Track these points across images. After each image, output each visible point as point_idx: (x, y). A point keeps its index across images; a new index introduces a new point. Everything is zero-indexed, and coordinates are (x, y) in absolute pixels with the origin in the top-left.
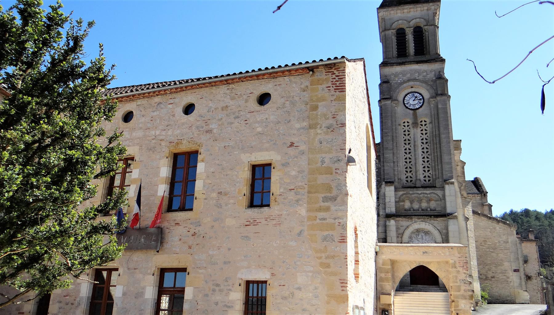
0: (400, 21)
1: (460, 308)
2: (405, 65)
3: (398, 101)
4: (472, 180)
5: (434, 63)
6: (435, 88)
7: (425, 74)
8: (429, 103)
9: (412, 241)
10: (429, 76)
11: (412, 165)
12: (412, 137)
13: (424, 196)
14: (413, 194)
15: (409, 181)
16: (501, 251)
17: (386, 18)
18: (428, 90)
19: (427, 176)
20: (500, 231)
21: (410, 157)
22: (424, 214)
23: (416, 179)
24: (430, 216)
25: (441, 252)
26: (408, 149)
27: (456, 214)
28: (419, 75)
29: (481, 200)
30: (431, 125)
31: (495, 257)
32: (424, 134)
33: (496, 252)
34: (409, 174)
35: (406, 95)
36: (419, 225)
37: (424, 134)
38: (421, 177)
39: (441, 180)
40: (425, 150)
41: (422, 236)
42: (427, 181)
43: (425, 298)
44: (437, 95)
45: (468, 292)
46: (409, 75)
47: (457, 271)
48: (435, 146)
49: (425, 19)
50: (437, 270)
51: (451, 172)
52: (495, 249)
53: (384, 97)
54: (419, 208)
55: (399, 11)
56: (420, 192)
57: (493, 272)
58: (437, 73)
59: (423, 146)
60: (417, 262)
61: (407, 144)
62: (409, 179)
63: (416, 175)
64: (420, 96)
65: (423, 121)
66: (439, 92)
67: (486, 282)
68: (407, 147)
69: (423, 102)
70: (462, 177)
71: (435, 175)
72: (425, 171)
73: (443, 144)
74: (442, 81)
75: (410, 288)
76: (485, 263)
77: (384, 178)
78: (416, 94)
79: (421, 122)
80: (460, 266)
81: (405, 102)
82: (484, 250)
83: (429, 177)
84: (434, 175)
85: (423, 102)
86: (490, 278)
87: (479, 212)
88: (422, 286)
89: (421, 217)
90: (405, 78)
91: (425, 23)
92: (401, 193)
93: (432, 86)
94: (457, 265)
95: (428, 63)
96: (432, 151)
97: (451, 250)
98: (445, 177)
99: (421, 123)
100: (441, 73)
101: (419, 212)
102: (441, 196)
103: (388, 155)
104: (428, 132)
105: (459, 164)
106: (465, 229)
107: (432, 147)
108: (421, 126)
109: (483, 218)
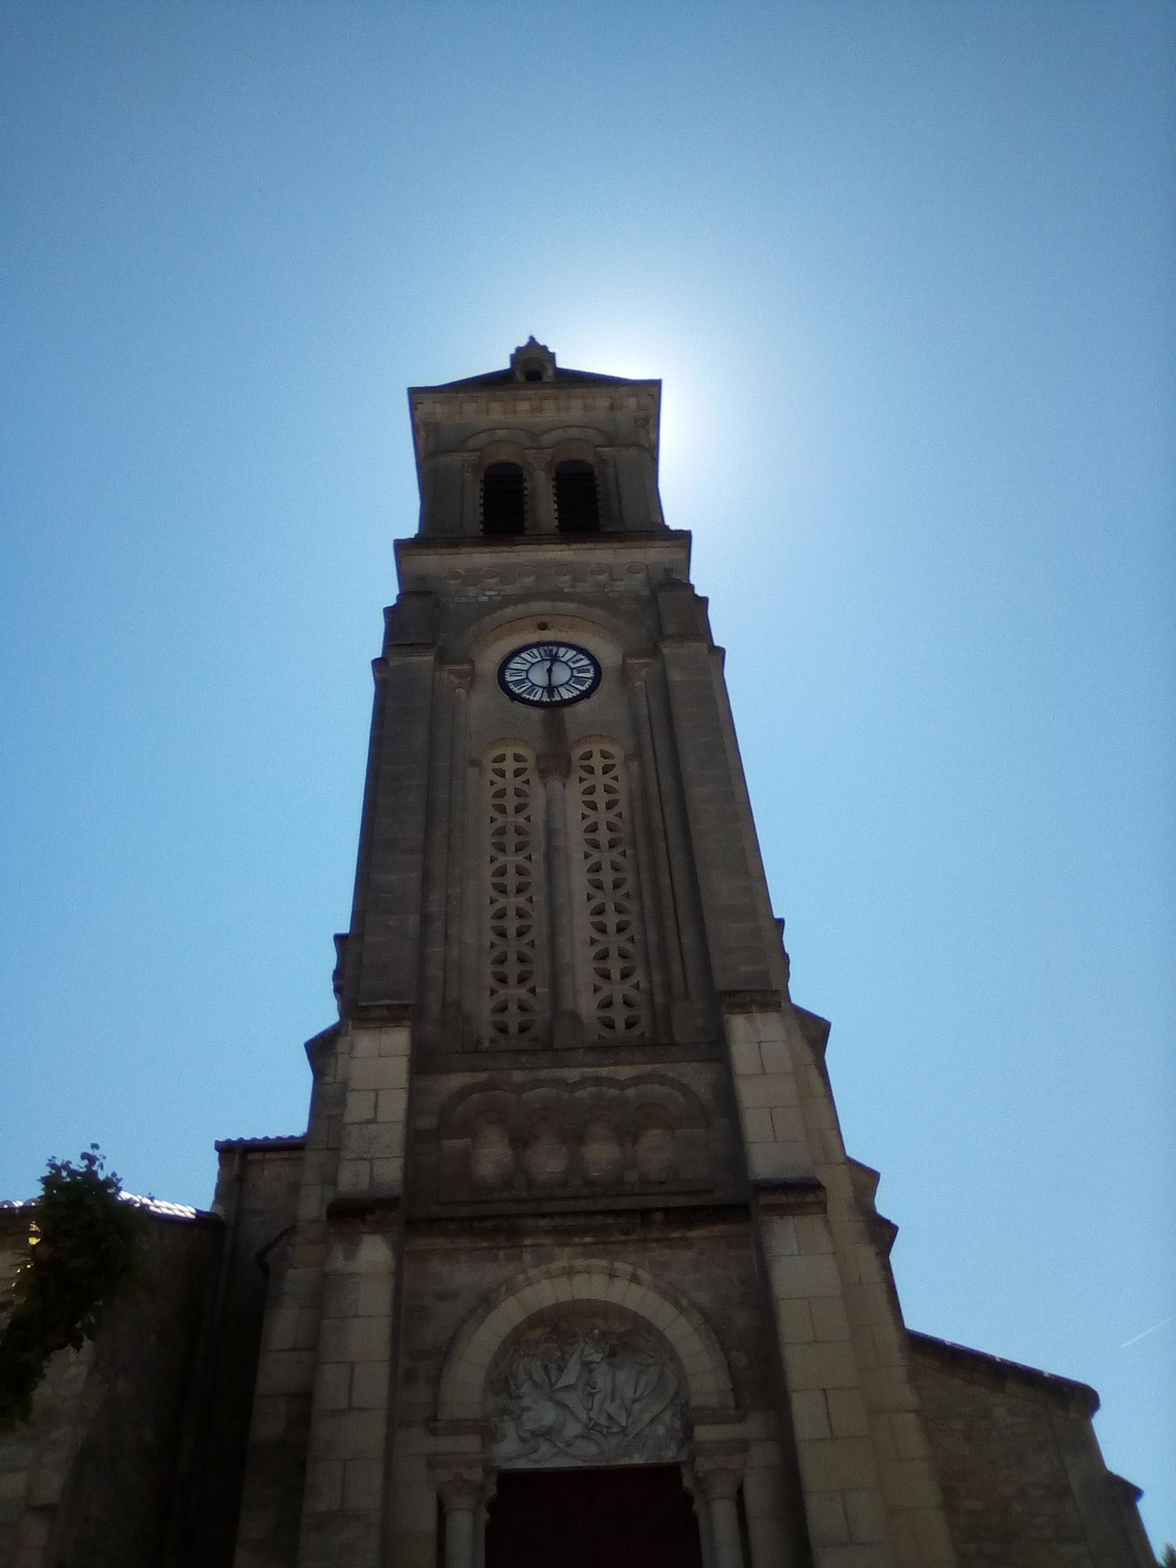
7: (603, 578)
10: (620, 586)
12: (538, 818)
14: (537, 1084)
30: (634, 765)
34: (515, 993)
38: (587, 1006)
41: (587, 1366)
42: (620, 1023)
46: (529, 581)
48: (662, 844)
49: (600, 431)
62: (513, 1019)
68: (511, 860)
71: (668, 987)
81: (509, 679)
90: (509, 590)
92: (455, 1082)
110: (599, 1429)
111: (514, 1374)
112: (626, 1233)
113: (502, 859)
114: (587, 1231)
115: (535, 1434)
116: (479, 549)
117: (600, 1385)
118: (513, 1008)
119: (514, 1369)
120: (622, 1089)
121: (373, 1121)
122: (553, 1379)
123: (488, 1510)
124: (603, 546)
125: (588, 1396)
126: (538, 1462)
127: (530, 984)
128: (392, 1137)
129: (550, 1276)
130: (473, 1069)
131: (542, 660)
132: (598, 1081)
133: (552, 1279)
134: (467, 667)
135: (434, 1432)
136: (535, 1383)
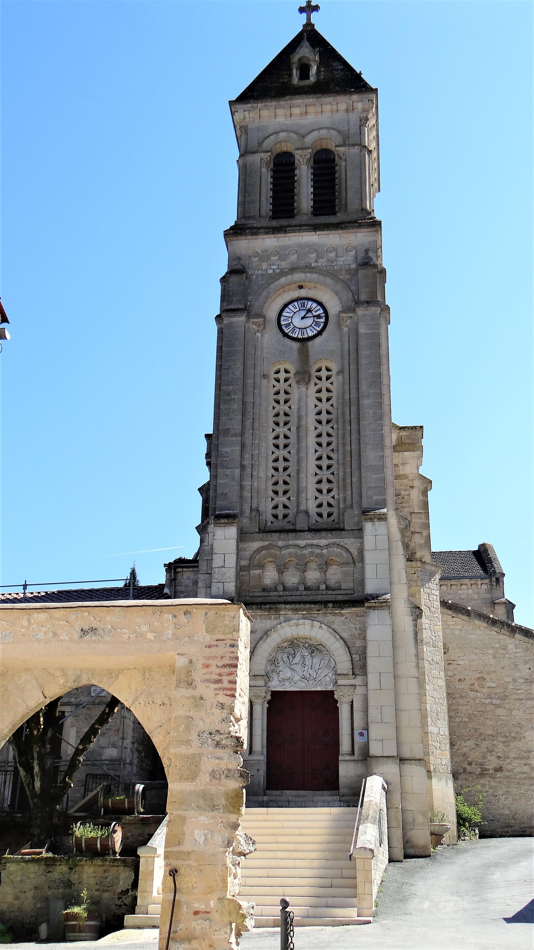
0: (283, 135)
1: (187, 846)
2: (286, 232)
3: (264, 317)
4: (474, 550)
5: (356, 230)
6: (353, 288)
8: (339, 325)
9: (277, 670)
11: (289, 475)
13: (312, 554)
14: (287, 547)
15: (280, 517)
16: (518, 704)
17: (250, 126)
18: (336, 293)
19: (325, 504)
20: (517, 655)
21: (288, 456)
22: (311, 598)
23: (298, 512)
24: (325, 603)
25: (145, 628)
26: (282, 436)
27: (388, 596)
28: (318, 257)
29: (491, 593)
30: (340, 377)
31: (505, 718)
32: (324, 400)
33: (507, 706)
34: (282, 499)
35: (286, 306)
36: (295, 627)
37: (324, 400)
38: (312, 506)
39: (356, 512)
40: (324, 440)
41: (303, 657)
42: (325, 515)
43: (279, 824)
44: (358, 303)
45: (224, 781)
46: (294, 258)
47: (194, 697)
48: (348, 428)
49: (339, 131)
50: (136, 698)
51: (383, 490)
52: (504, 698)
53: (229, 307)
54: (299, 583)
55: (280, 112)
56: (302, 543)
57: (499, 757)
58: (362, 255)
59: (320, 428)
60: (70, 673)
61: (282, 424)
62: (281, 512)
63: (297, 499)
64: (319, 307)
65: (324, 369)
66: (363, 297)
67: (482, 781)
68: (281, 430)
69: (326, 323)
70: (423, 516)
71: (345, 500)
72: (320, 491)
73: (365, 422)
74: (370, 271)
75: (260, 798)
76: (481, 734)
77: (215, 508)
78: (310, 304)
79: (319, 370)
80: (208, 677)
81: (283, 323)
82: (478, 701)
83: (329, 505)
84: (341, 501)
85: (326, 323)
86: (491, 772)
87: (469, 608)
88: (295, 792)
89: (302, 606)
90: (284, 264)
91: (339, 140)
93: (346, 284)
94: (198, 675)
95: (342, 228)
96: (340, 440)
97: (183, 619)
98: (365, 505)
99: (318, 374)
100: (371, 254)
101: (298, 593)
102: (355, 552)
103: (228, 450)
104: (334, 395)
105: (417, 483)
106: (411, 635)
107: (340, 432)
108: (317, 381)
109: (477, 622)
112: (319, 610)
113: (278, 430)
116: (268, 236)
117: (307, 663)
118: (281, 507)
122: (291, 661)
123: (268, 703)
124: (333, 232)
127: (288, 495)
128: (231, 574)
130: (262, 540)
131: (300, 310)
132: (312, 545)
134: (261, 320)
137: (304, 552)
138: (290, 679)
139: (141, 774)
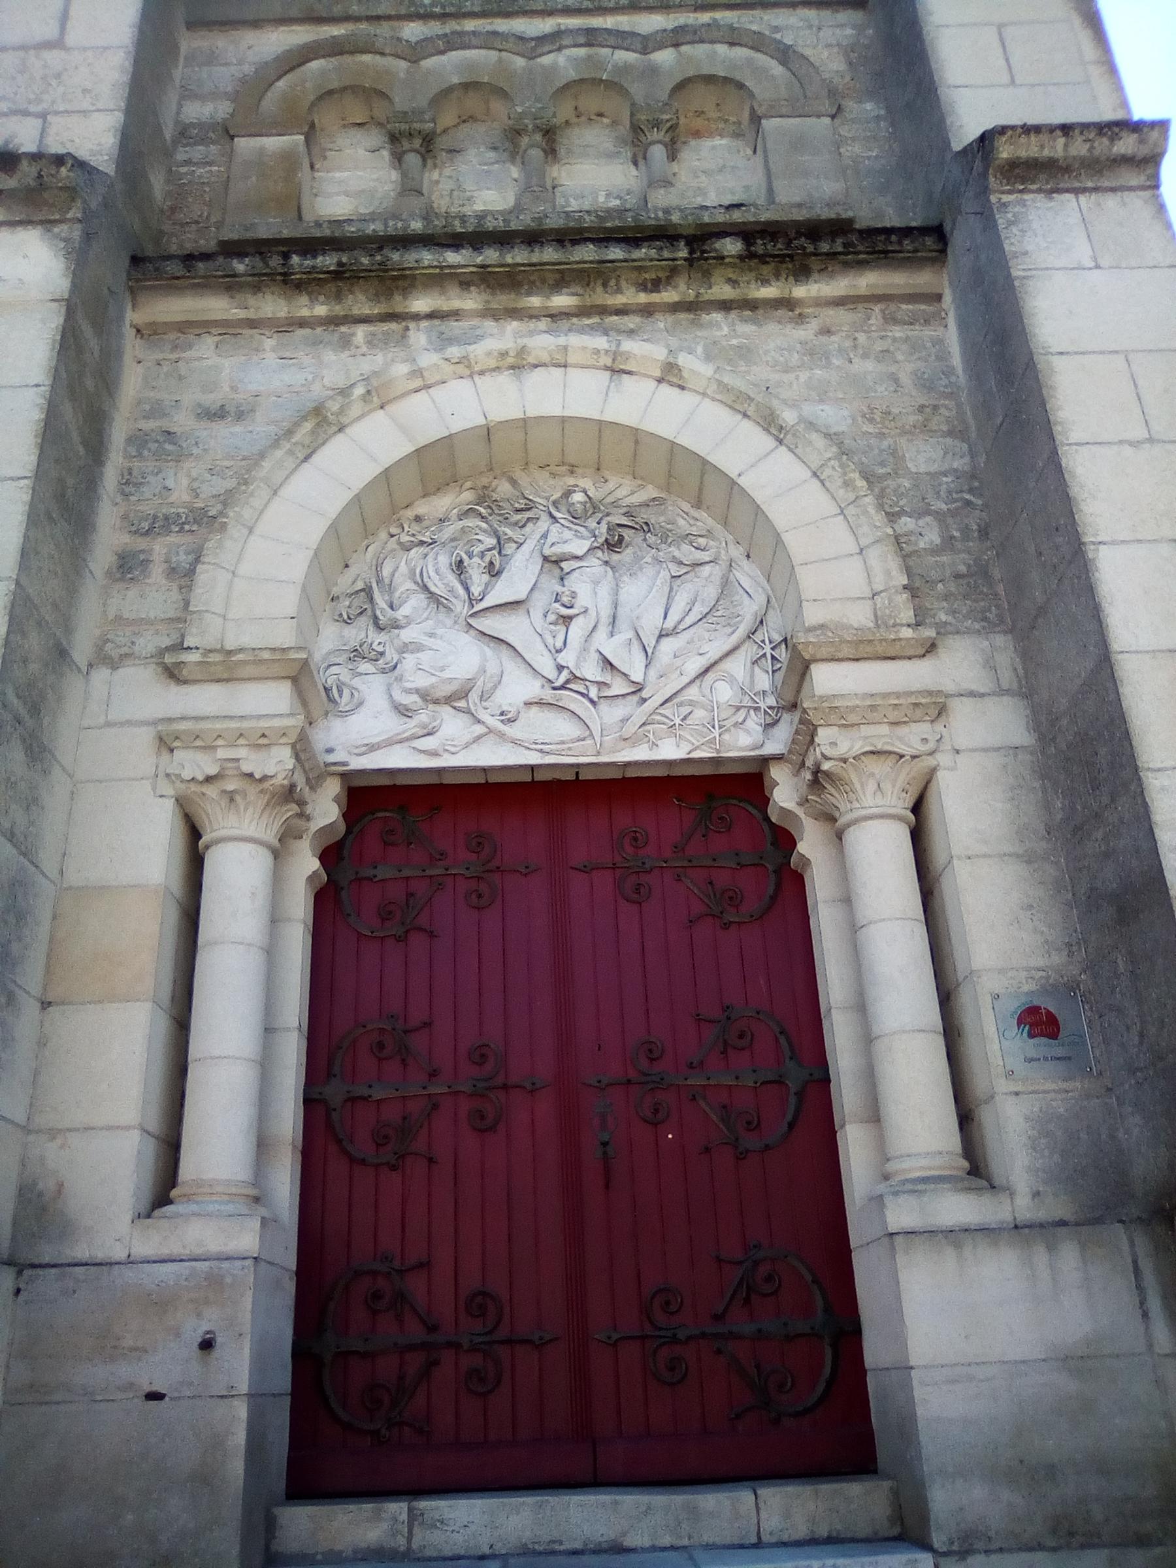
110: (582, 689)
111: (387, 581)
114: (562, 279)
115: (428, 698)
117: (583, 600)
119: (386, 572)
120: (645, 51)
121: (57, 44)
122: (476, 590)
125: (555, 623)
126: (434, 754)
129: (469, 370)
132: (591, 37)
133: (476, 378)
135: (173, 674)
136: (434, 598)
137: (546, 60)
138: (474, 696)
139: (1042, 932)
